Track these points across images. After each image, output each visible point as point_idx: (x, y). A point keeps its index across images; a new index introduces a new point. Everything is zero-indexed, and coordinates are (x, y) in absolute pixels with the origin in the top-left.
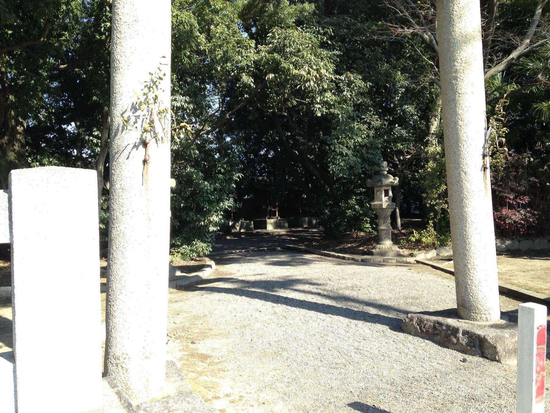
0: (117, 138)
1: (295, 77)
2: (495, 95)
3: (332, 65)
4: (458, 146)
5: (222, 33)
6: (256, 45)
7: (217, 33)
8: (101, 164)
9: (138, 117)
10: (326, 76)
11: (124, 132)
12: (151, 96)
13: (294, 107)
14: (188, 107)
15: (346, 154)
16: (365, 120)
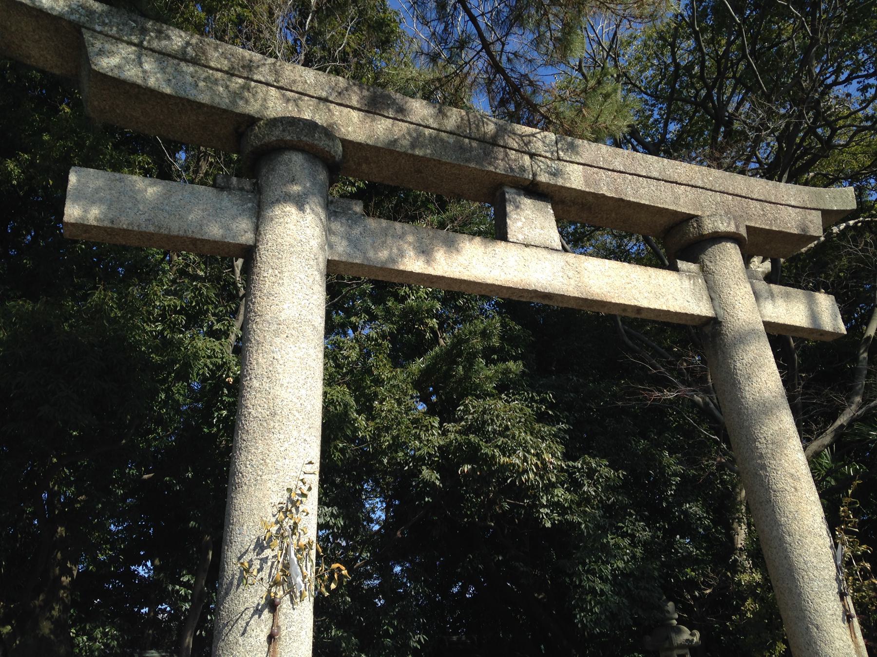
0: (228, 598)
1: (504, 467)
2: (828, 482)
3: (560, 447)
4: (794, 580)
5: (390, 411)
6: (441, 424)
7: (382, 411)
8: (189, 633)
9: (264, 560)
10: (551, 463)
11: (242, 587)
12: (288, 523)
13: (504, 512)
14: (335, 524)
15: (602, 590)
16: (625, 529)
